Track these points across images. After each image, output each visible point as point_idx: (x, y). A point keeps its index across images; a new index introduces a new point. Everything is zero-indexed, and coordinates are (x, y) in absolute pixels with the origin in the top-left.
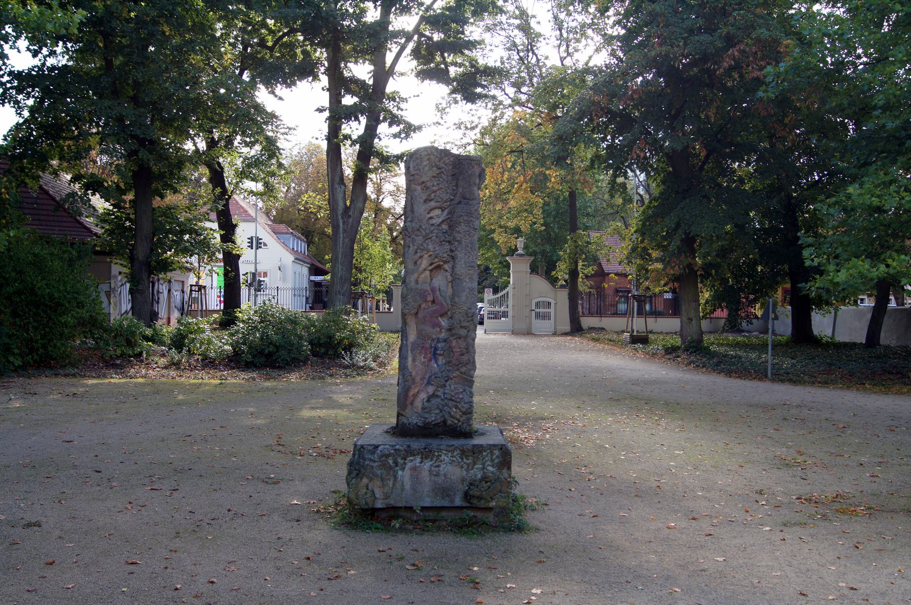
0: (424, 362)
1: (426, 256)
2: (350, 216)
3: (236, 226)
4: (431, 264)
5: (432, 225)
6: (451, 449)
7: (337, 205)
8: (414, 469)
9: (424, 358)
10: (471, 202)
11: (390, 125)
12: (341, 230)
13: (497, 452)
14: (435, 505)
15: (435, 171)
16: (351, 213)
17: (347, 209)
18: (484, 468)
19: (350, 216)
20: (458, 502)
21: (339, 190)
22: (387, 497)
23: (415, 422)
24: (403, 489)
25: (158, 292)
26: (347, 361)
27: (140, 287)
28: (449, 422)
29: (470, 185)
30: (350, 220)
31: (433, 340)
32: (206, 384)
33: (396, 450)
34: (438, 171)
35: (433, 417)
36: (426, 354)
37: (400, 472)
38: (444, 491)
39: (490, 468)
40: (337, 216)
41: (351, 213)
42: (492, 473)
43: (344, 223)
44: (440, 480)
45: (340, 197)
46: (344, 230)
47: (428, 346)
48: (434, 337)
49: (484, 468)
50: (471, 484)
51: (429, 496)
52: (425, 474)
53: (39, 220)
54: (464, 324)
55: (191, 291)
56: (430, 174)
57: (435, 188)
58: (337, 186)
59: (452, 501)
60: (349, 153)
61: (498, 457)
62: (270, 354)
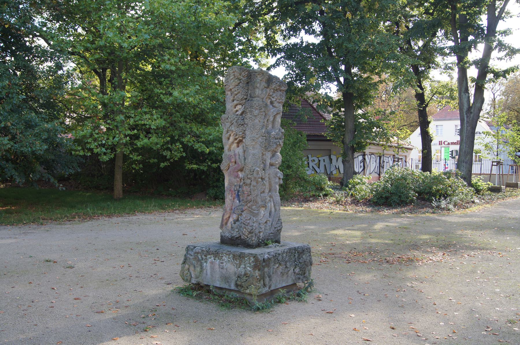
0: (231, 199)
1: (232, 134)
2: (471, 113)
3: (430, 122)
4: (236, 139)
5: (237, 115)
6: (229, 253)
7: (463, 106)
8: (212, 263)
9: (231, 196)
10: (254, 99)
11: (500, 50)
12: (465, 121)
13: (252, 259)
14: (221, 286)
15: (237, 81)
16: (472, 111)
17: (470, 108)
18: (245, 268)
19: (471, 113)
20: (233, 287)
21: (464, 97)
22: (197, 278)
23: (227, 235)
24: (207, 274)
25: (384, 162)
26: (434, 204)
27: (347, 159)
28: (242, 237)
29: (254, 88)
30: (472, 115)
31: (235, 186)
32: (324, 213)
33: (202, 250)
34: (238, 82)
35: (235, 234)
36: (232, 194)
37: (205, 264)
38: (226, 279)
39: (248, 268)
40: (463, 113)
41: (472, 111)
42: (250, 271)
43: (467, 117)
44: (224, 271)
45: (465, 101)
46: (467, 122)
47: (233, 189)
48: (236, 184)
49: (245, 268)
50: (239, 277)
51: (218, 281)
52: (217, 266)
53: (310, 124)
54: (249, 176)
55: (492, 165)
56: (234, 84)
57: (236, 92)
58: (463, 94)
59: (230, 286)
60: (473, 72)
61: (253, 262)
62: (387, 198)
